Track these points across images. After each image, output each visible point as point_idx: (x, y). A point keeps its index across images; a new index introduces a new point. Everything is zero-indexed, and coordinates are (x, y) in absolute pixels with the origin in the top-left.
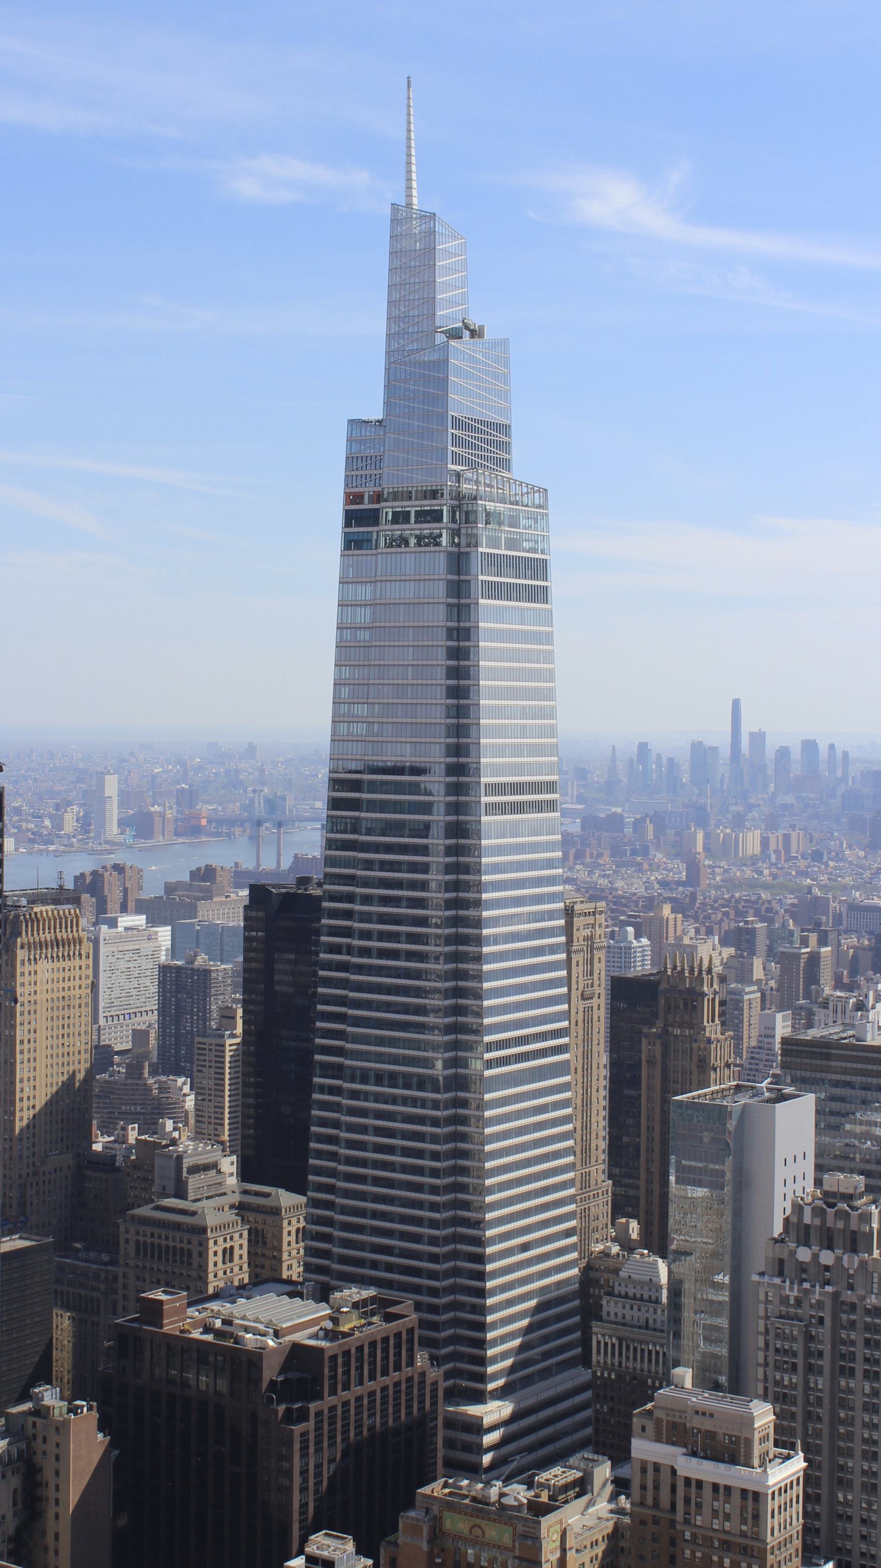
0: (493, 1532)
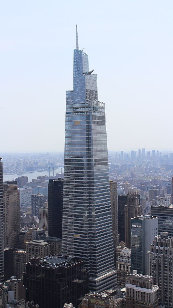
0: (100, 302)
